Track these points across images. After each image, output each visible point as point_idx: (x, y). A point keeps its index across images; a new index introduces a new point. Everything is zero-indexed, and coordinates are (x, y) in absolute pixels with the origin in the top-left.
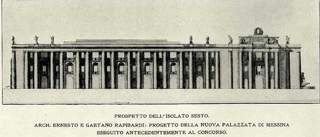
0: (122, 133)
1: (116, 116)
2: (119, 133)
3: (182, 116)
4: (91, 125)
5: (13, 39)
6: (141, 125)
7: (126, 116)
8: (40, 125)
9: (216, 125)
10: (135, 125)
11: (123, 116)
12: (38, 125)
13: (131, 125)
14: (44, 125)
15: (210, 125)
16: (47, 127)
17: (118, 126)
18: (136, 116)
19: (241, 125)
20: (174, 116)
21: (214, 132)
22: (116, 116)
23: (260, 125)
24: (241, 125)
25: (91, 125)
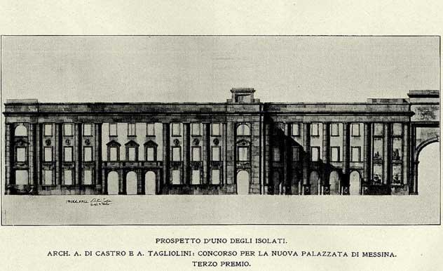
0: (214, 264)
2: (194, 241)
3: (277, 241)
4: (103, 253)
7: (173, 241)
8: (55, 253)
12: (53, 254)
16: (66, 256)
18: (185, 241)
19: (327, 254)
20: (267, 241)
21: (205, 254)
22: (157, 241)
23: (87, 253)
24: (327, 254)
25: (103, 253)
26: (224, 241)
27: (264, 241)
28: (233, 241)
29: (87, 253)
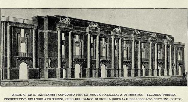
1: (5, 99)
2: (150, 99)
3: (47, 99)
4: (86, 99)
5: (181, 99)
6: (53, 95)
9: (99, 95)
10: (49, 95)
11: (9, 99)
13: (47, 95)
14: (18, 95)
15: (95, 95)
17: (40, 95)
18: (158, 99)
19: (113, 95)
22: (5, 99)
23: (125, 95)
24: (113, 95)
25: (86, 99)
26: (167, 99)
27: (41, 99)
28: (29, 99)
29: (125, 95)
